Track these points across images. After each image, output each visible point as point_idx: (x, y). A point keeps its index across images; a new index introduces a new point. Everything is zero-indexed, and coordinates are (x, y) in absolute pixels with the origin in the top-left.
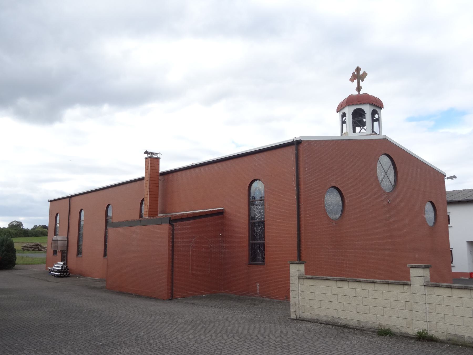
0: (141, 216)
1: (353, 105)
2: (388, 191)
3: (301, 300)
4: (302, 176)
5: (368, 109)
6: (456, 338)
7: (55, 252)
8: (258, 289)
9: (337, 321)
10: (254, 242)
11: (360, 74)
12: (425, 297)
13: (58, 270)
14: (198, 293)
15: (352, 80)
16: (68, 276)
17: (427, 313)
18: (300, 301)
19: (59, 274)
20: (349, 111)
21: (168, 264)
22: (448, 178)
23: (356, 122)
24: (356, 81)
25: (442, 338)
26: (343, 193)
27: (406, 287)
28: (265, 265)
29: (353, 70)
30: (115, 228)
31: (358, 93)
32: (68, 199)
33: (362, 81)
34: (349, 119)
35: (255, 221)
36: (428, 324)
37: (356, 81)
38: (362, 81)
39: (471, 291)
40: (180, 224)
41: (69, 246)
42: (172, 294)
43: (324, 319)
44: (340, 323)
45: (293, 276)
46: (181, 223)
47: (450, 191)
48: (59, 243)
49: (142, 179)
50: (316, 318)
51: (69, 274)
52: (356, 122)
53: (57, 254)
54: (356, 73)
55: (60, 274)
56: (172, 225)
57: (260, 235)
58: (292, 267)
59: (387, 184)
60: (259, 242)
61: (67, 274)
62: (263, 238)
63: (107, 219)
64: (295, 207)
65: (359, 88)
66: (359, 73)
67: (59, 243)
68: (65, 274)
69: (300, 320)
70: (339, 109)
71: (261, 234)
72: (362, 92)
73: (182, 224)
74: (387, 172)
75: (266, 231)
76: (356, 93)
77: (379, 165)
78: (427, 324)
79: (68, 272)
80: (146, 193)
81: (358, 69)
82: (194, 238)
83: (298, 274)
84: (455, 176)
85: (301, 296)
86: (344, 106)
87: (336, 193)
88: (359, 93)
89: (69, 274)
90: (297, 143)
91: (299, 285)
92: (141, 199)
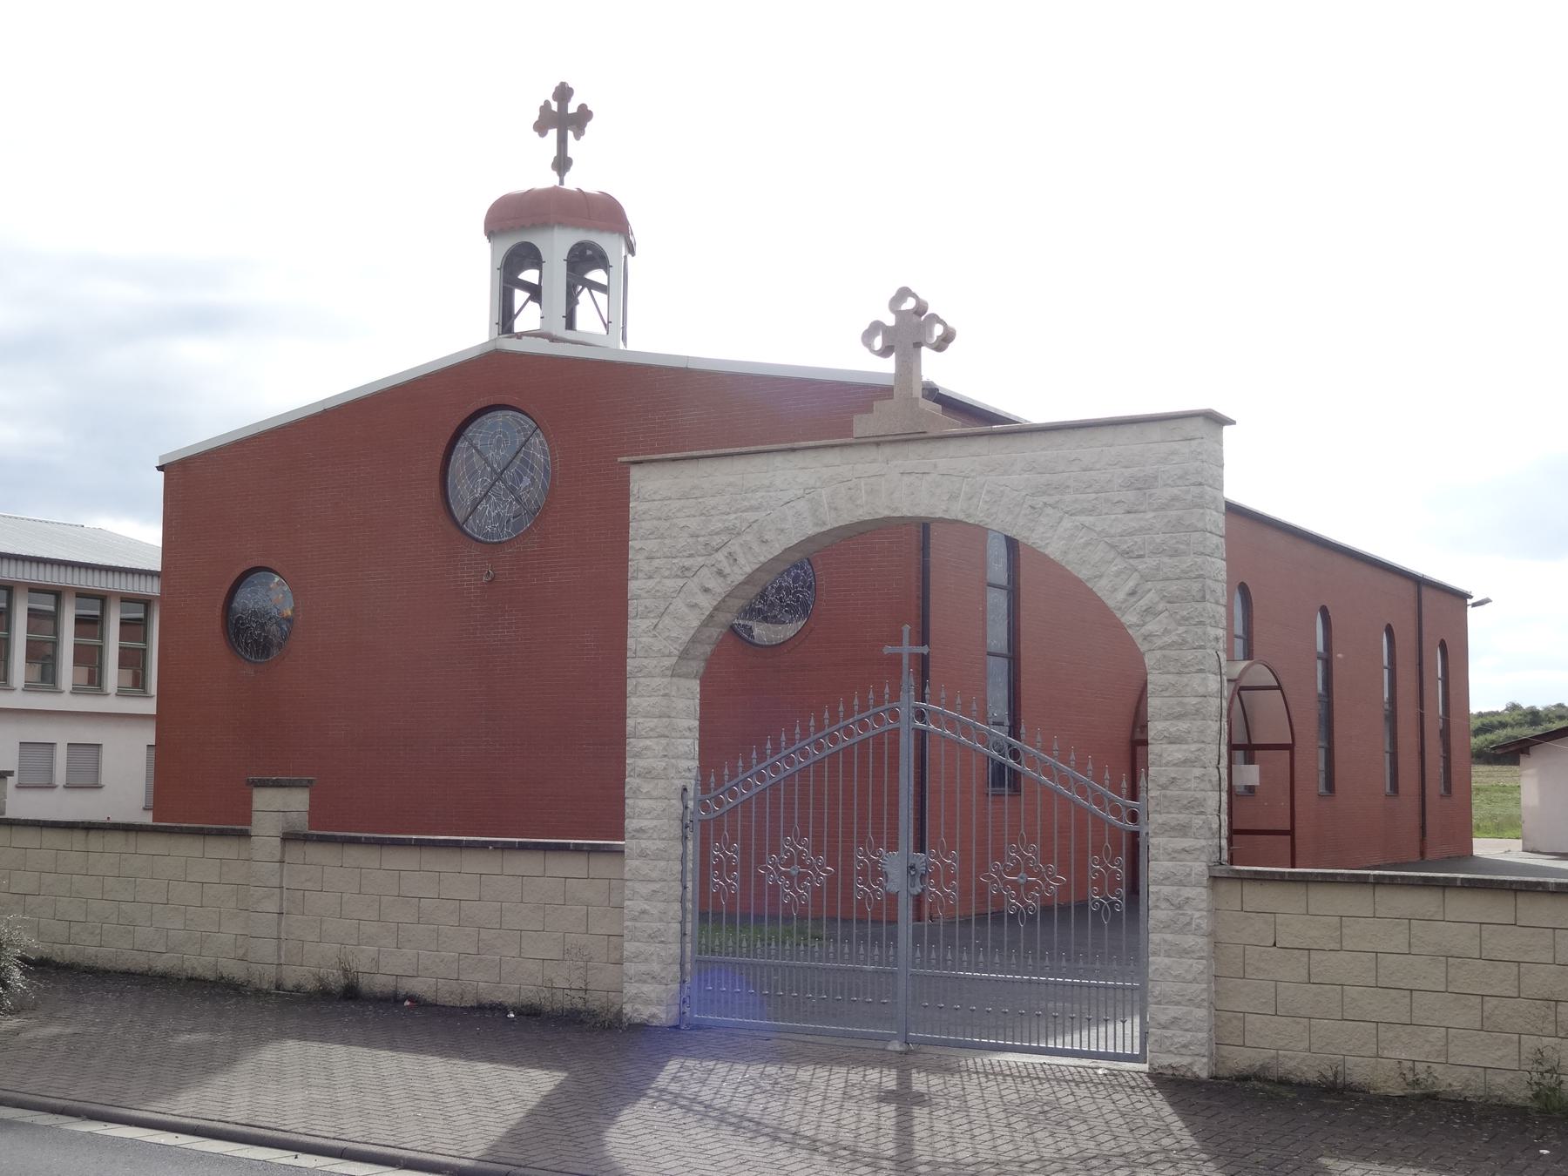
11: (556, 130)
15: (541, 128)
21: (911, 1134)
24: (553, 133)
29: (548, 94)
31: (557, 178)
33: (577, 137)
37: (553, 133)
38: (577, 137)
39: (545, 854)
54: (554, 106)
59: (498, 514)
65: (562, 164)
72: (572, 182)
76: (548, 180)
81: (563, 93)
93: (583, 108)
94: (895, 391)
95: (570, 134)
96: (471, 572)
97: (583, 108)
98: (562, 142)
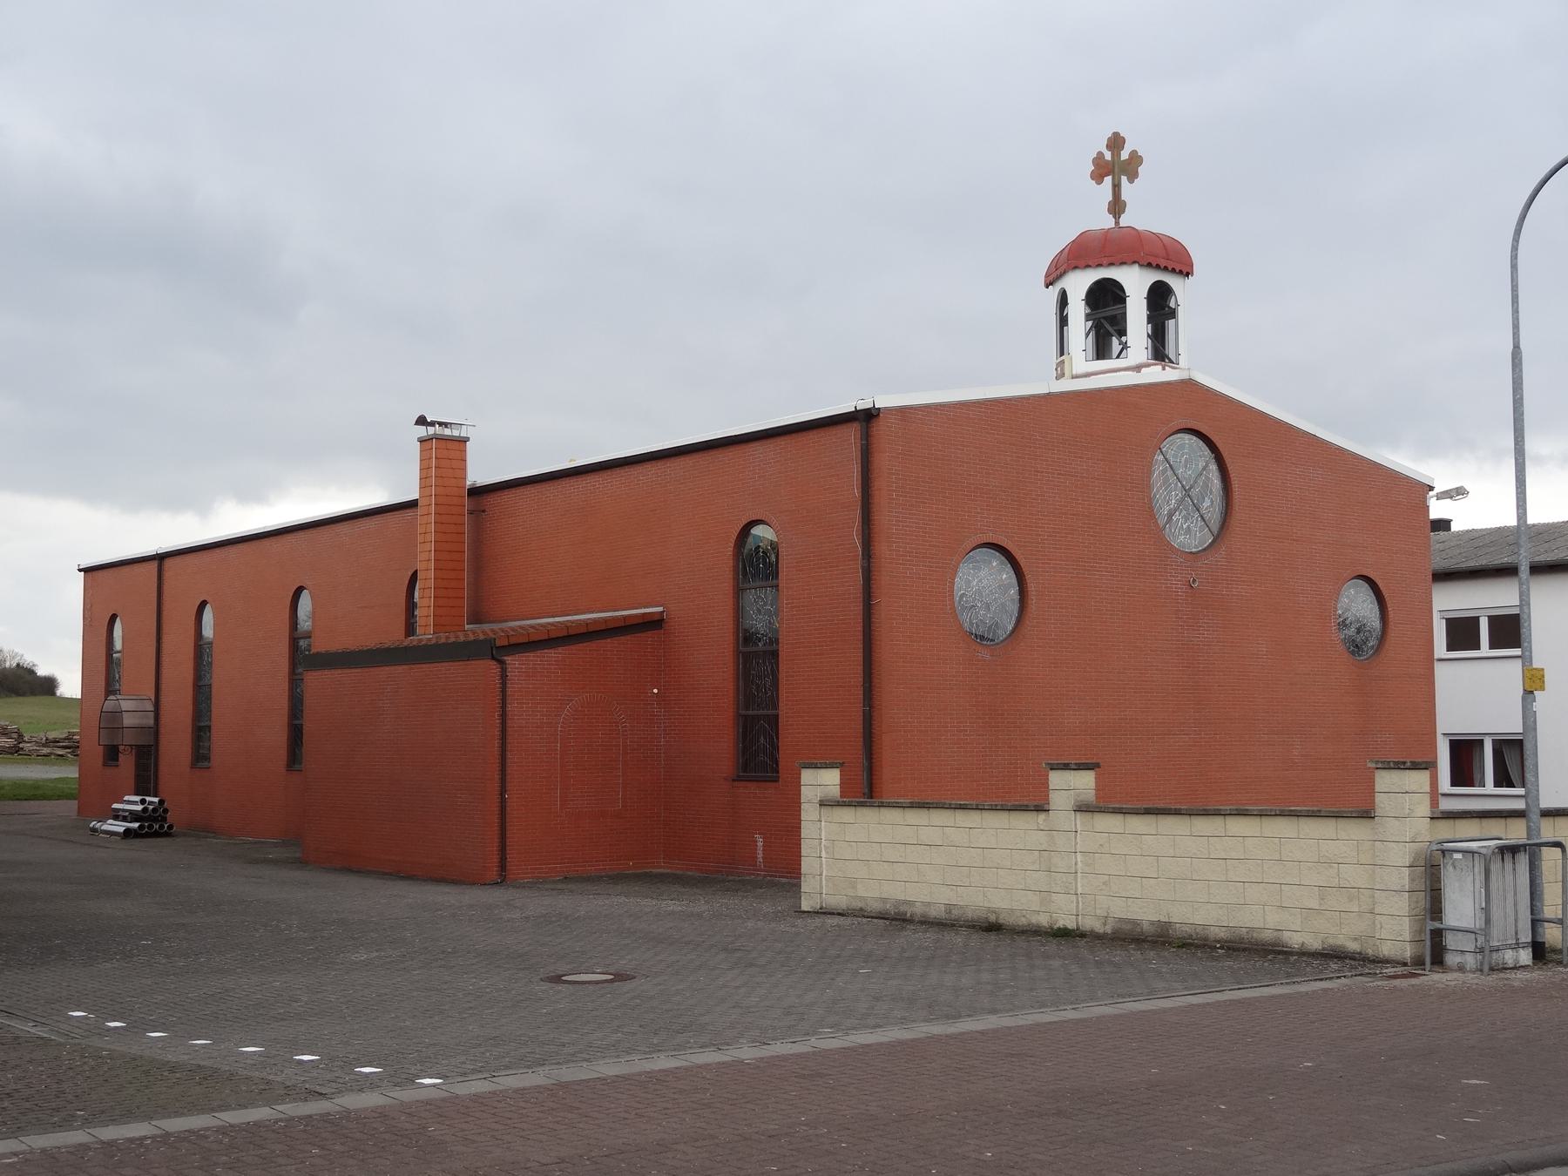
0: (410, 629)
1: (1158, 267)
2: (1194, 550)
3: (826, 862)
4: (885, 516)
5: (1135, 283)
6: (1129, 927)
7: (112, 754)
8: (760, 852)
9: (902, 908)
10: (750, 712)
12: (1076, 838)
13: (131, 812)
14: (585, 866)
15: (1098, 177)
16: (167, 835)
17: (1079, 875)
18: (824, 866)
19: (136, 825)
20: (1079, 284)
22: (1440, 497)
23: (1102, 321)
25: (1098, 927)
26: (1022, 562)
27: (1042, 816)
28: (777, 781)
30: (326, 672)
32: (154, 565)
33: (1131, 180)
34: (1077, 310)
35: (754, 649)
36: (1080, 899)
37: (1108, 180)
38: (1131, 180)
40: (526, 660)
41: (162, 730)
42: (503, 866)
43: (875, 906)
44: (908, 915)
45: (809, 802)
46: (528, 656)
47: (1551, 522)
48: (128, 721)
49: (412, 504)
50: (860, 905)
51: (170, 827)
52: (1102, 321)
53: (120, 759)
54: (1108, 156)
55: (139, 826)
56: (502, 662)
57: (766, 693)
58: (807, 776)
59: (1188, 526)
60: (765, 712)
61: (162, 827)
62: (774, 703)
63: (296, 636)
64: (857, 609)
65: (1117, 207)
66: (1119, 155)
67: (128, 721)
68: (156, 826)
69: (823, 912)
70: (1054, 275)
71: (769, 689)
72: (1125, 221)
73: (532, 661)
74: (1190, 489)
75: (782, 676)
76: (1108, 222)
77: (1159, 467)
78: (1078, 899)
79: (165, 819)
80: (424, 556)
81: (1116, 142)
82: (572, 700)
83: (820, 797)
84: (1462, 488)
85: (827, 853)
86: (1061, 270)
87: (996, 561)
88: (1117, 223)
89: (170, 827)
90: (866, 418)
91: (823, 823)
92: (410, 574)
93: (1134, 154)
94: (1441, 533)
95: (1124, 179)
96: (1177, 577)
97: (1134, 154)
98: (1116, 188)
